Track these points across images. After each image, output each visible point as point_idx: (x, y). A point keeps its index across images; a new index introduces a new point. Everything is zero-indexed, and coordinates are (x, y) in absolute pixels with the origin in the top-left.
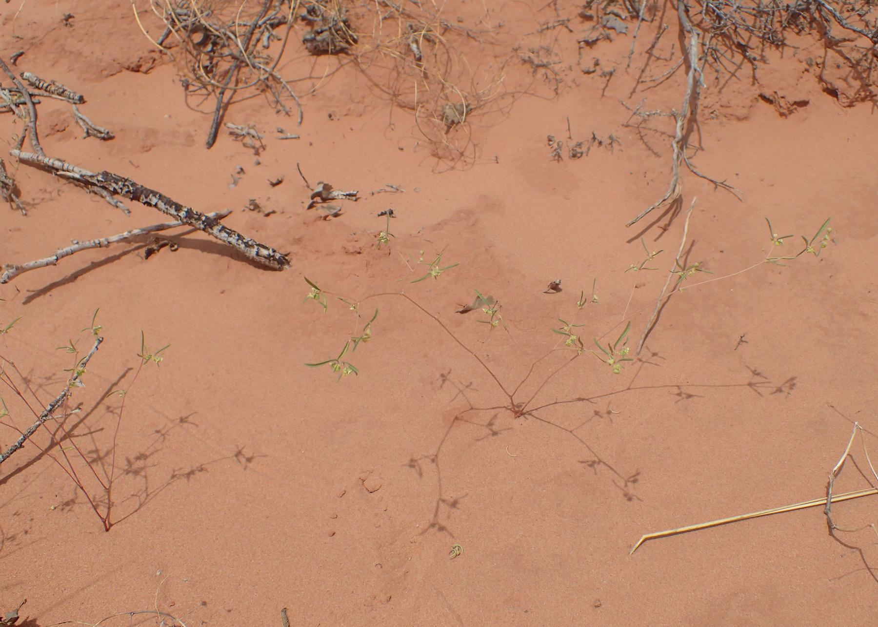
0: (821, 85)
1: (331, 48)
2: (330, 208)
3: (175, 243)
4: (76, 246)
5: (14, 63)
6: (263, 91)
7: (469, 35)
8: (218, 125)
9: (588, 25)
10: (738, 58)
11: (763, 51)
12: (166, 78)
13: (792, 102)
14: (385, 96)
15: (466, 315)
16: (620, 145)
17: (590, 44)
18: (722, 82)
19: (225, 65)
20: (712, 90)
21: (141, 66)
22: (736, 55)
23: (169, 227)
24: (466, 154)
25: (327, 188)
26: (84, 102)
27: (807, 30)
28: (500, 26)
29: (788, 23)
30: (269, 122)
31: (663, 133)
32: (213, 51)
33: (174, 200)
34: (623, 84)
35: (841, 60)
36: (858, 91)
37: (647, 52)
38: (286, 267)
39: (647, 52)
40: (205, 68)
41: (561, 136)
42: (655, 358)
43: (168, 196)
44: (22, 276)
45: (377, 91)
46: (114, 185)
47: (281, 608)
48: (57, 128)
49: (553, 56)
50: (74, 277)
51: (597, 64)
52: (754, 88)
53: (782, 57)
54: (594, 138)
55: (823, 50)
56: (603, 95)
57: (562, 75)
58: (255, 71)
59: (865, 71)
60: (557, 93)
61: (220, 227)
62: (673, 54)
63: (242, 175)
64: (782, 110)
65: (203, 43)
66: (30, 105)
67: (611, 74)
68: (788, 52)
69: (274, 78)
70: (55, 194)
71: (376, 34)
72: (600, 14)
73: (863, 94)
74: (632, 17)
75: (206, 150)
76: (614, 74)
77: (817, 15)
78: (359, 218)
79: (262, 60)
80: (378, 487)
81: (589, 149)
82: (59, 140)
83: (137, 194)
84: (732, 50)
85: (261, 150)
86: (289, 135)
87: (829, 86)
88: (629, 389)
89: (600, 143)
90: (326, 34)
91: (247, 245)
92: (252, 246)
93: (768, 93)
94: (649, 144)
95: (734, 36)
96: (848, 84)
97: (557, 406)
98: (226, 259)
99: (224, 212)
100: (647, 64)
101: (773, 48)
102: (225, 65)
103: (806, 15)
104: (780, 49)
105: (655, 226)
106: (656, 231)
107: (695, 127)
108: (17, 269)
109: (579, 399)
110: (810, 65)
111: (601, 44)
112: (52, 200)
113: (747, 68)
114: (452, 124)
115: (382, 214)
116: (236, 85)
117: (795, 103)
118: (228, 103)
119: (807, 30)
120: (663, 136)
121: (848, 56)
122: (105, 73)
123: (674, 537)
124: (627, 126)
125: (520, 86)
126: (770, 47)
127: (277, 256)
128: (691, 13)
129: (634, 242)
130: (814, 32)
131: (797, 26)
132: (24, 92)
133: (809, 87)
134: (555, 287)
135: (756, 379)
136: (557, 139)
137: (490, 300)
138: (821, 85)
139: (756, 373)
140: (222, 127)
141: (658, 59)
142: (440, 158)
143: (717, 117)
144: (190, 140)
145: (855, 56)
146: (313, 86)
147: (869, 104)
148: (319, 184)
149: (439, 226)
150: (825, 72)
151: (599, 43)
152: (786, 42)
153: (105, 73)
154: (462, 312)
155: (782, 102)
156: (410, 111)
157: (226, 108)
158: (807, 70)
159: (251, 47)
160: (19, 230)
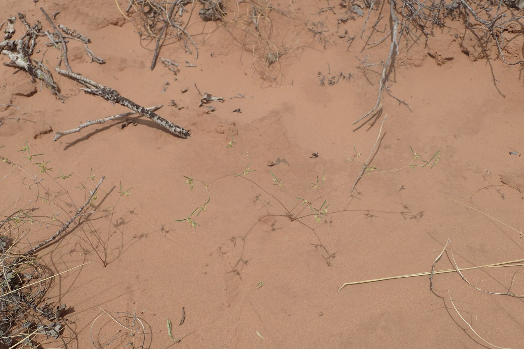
1: (213, 18)
2: (210, 107)
3: (135, 121)
4: (89, 123)
5: (55, 18)
6: (178, 40)
7: (283, 14)
8: (157, 57)
9: (344, 10)
10: (420, 32)
11: (432, 29)
12: (130, 32)
14: (239, 45)
15: (272, 167)
16: (354, 78)
18: (409, 46)
19: (160, 25)
21: (118, 22)
22: (419, 30)
23: (133, 114)
24: (278, 80)
25: (209, 96)
26: (90, 42)
27: (457, 18)
28: (299, 9)
29: (448, 14)
30: (182, 57)
31: (376, 73)
32: (154, 17)
33: (136, 103)
34: (359, 44)
35: (473, 36)
36: (480, 53)
38: (188, 137)
40: (150, 26)
41: (325, 73)
43: (133, 101)
44: (63, 137)
45: (235, 42)
46: (107, 96)
47: (181, 307)
48: (77, 56)
49: (324, 27)
50: (88, 137)
51: (346, 33)
52: (426, 49)
54: (341, 75)
55: (464, 29)
58: (175, 29)
59: (484, 43)
61: (157, 117)
62: (386, 29)
63: (168, 86)
64: (439, 62)
65: (149, 12)
66: (63, 43)
67: (353, 39)
68: (446, 30)
69: (184, 33)
70: (77, 92)
71: (236, 11)
72: (351, 5)
73: (482, 55)
74: (367, 7)
75: (150, 71)
77: (463, 11)
78: (224, 112)
79: (178, 23)
81: (338, 80)
82: (79, 63)
83: (118, 100)
84: (417, 28)
85: (177, 72)
86: (191, 65)
89: (344, 77)
90: (211, 10)
91: (170, 126)
92: (172, 127)
94: (369, 78)
95: (418, 20)
98: (160, 131)
99: (159, 106)
100: (372, 34)
101: (438, 28)
102: (160, 25)
103: (458, 10)
105: (367, 123)
106: (367, 126)
107: (393, 70)
108: (61, 134)
110: (457, 38)
111: (350, 22)
112: (76, 95)
113: (423, 39)
115: (235, 111)
116: (166, 37)
117: (446, 59)
118: (162, 46)
119: (457, 18)
120: (377, 74)
122: (100, 26)
124: (359, 68)
127: (184, 132)
128: (397, 7)
129: (356, 131)
130: (461, 20)
131: (452, 16)
132: (61, 37)
134: (316, 155)
135: (406, 210)
136: (323, 74)
137: (284, 160)
139: (406, 207)
140: (158, 60)
141: (378, 31)
142: (264, 80)
144: (142, 65)
145: (480, 34)
146: (204, 38)
147: (485, 60)
148: (205, 94)
149: (262, 120)
150: (464, 42)
151: (348, 21)
152: (445, 25)
153: (100, 26)
154: (270, 166)
155: (439, 58)
157: (160, 48)
158: (455, 41)
159: (173, 16)
160: (61, 111)
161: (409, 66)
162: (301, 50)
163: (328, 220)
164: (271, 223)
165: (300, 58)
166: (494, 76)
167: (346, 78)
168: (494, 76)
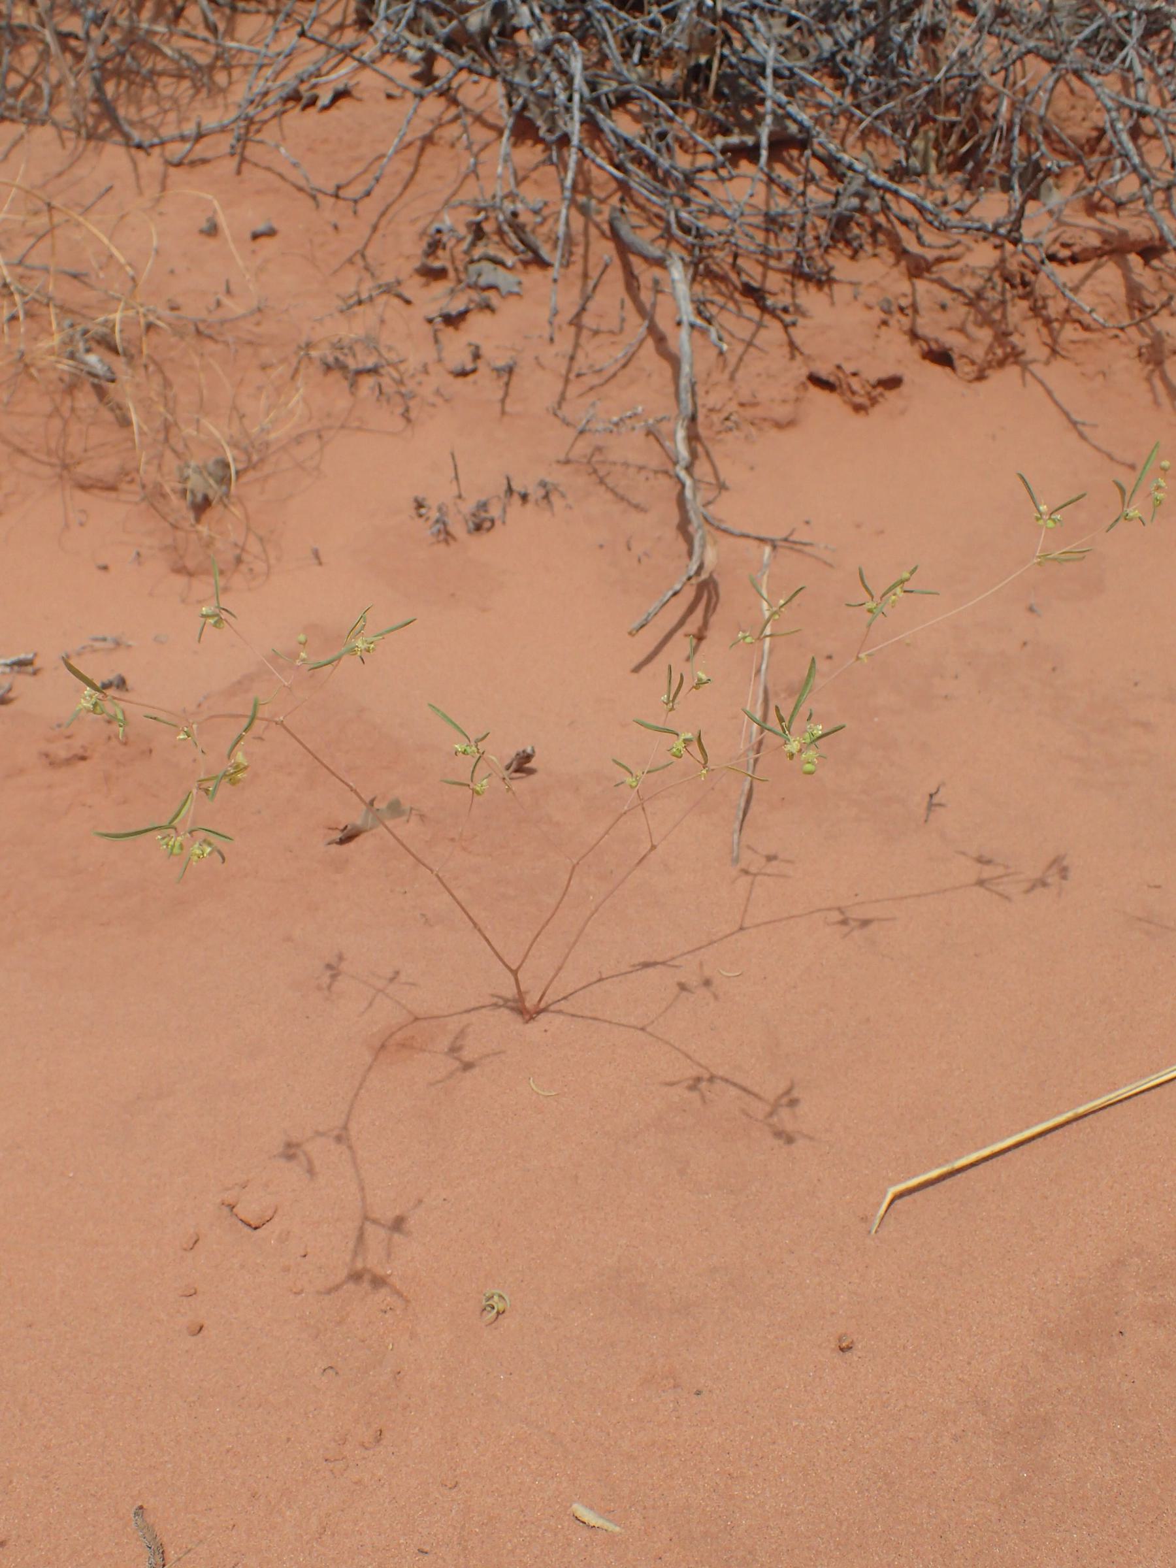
0: (916, 348)
7: (198, 332)
9: (440, 288)
10: (753, 312)
11: (794, 296)
13: (873, 380)
14: (46, 471)
17: (453, 320)
18: (732, 360)
20: (717, 376)
27: (868, 248)
29: (832, 238)
31: (641, 468)
34: (538, 388)
35: (945, 296)
36: (991, 347)
37: (571, 323)
39: (571, 323)
41: (440, 493)
42: (774, 863)
45: (23, 463)
51: (477, 356)
53: (833, 304)
54: (510, 490)
56: (503, 413)
57: (411, 385)
59: (995, 308)
60: (409, 420)
62: (623, 320)
64: (858, 400)
67: (510, 370)
68: (842, 292)
73: (999, 352)
74: (525, 264)
76: (517, 370)
80: (270, 1213)
84: (736, 302)
87: (934, 346)
88: (741, 929)
93: (824, 370)
94: (620, 491)
95: (733, 276)
96: (968, 336)
97: (606, 985)
100: (577, 345)
101: (813, 289)
104: (826, 289)
105: (679, 635)
106: (682, 643)
107: (700, 449)
109: (646, 965)
110: (888, 312)
113: (773, 332)
114: (202, 506)
119: (868, 248)
120: (643, 474)
121: (957, 285)
123: (948, 1182)
124: (567, 462)
125: (329, 415)
126: (806, 287)
129: (645, 669)
130: (884, 251)
131: (848, 243)
133: (895, 353)
134: (522, 764)
135: (987, 872)
136: (432, 502)
138: (916, 348)
139: (980, 860)
141: (596, 333)
143: (737, 426)
145: (970, 284)
147: (1013, 371)
150: (920, 321)
152: (834, 274)
154: (342, 842)
155: (855, 384)
156: (105, 494)
158: (885, 323)
161: (753, 430)
162: (313, 444)
163: (694, 981)
164: (445, 1043)
165: (317, 468)
166: (1067, 414)
167: (531, 498)
168: (1067, 414)
